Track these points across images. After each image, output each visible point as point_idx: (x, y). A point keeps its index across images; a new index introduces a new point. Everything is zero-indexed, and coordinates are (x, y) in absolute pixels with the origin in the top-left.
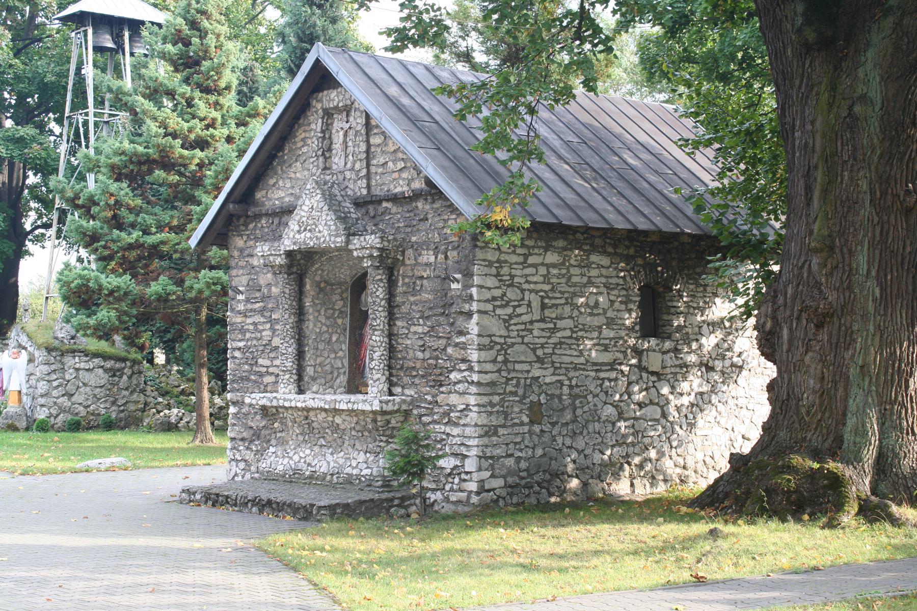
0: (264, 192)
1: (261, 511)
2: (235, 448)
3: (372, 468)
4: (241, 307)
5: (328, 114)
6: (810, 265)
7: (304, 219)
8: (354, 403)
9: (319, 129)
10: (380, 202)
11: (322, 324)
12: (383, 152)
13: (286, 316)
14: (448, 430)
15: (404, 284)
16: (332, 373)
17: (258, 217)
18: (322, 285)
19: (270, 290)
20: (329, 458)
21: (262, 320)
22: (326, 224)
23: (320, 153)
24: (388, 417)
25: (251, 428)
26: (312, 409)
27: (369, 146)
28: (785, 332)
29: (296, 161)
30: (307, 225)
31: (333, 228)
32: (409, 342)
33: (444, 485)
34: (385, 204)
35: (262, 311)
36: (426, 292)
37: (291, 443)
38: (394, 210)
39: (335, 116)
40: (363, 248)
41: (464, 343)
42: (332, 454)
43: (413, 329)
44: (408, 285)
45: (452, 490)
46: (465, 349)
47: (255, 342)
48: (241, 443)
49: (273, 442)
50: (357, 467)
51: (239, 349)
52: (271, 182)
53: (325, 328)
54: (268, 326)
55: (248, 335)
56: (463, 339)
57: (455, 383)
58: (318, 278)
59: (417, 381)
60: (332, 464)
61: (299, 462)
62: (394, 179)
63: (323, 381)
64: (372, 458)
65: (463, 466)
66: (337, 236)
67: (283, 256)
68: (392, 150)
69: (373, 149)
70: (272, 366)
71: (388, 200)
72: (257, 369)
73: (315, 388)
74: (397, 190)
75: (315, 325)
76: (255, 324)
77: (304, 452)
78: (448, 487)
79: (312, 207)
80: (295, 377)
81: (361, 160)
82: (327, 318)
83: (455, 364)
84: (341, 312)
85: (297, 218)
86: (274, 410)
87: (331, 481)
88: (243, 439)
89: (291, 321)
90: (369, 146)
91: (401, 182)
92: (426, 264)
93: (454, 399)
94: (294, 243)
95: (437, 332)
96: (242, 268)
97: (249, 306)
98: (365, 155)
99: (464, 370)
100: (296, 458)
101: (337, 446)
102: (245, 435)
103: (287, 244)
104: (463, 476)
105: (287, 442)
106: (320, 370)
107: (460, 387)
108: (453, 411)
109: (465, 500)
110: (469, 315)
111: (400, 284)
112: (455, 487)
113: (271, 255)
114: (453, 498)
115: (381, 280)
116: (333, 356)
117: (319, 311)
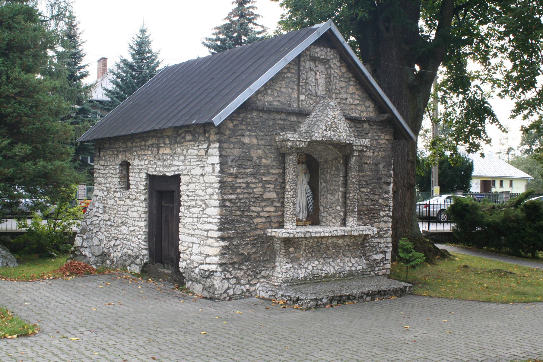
1: (373, 299)
2: (225, 270)
3: (362, 265)
7: (330, 123)
8: (363, 231)
14: (378, 240)
19: (260, 161)
20: (333, 264)
21: (254, 180)
25: (243, 254)
26: (324, 237)
35: (254, 175)
37: (301, 259)
40: (361, 146)
41: (388, 197)
42: (333, 261)
43: (362, 190)
45: (380, 270)
46: (388, 200)
47: (247, 196)
50: (353, 266)
54: (260, 185)
55: (239, 191)
56: (387, 196)
59: (363, 217)
60: (336, 268)
61: (313, 269)
64: (359, 260)
66: (351, 137)
68: (351, 92)
70: (263, 211)
72: (249, 214)
74: (353, 115)
77: (314, 263)
78: (377, 269)
79: (335, 118)
87: (340, 277)
88: (233, 264)
91: (357, 111)
92: (368, 157)
94: (323, 137)
95: (375, 192)
97: (243, 171)
100: (310, 268)
101: (334, 256)
105: (299, 259)
107: (385, 219)
108: (381, 231)
112: (381, 268)
114: (380, 274)
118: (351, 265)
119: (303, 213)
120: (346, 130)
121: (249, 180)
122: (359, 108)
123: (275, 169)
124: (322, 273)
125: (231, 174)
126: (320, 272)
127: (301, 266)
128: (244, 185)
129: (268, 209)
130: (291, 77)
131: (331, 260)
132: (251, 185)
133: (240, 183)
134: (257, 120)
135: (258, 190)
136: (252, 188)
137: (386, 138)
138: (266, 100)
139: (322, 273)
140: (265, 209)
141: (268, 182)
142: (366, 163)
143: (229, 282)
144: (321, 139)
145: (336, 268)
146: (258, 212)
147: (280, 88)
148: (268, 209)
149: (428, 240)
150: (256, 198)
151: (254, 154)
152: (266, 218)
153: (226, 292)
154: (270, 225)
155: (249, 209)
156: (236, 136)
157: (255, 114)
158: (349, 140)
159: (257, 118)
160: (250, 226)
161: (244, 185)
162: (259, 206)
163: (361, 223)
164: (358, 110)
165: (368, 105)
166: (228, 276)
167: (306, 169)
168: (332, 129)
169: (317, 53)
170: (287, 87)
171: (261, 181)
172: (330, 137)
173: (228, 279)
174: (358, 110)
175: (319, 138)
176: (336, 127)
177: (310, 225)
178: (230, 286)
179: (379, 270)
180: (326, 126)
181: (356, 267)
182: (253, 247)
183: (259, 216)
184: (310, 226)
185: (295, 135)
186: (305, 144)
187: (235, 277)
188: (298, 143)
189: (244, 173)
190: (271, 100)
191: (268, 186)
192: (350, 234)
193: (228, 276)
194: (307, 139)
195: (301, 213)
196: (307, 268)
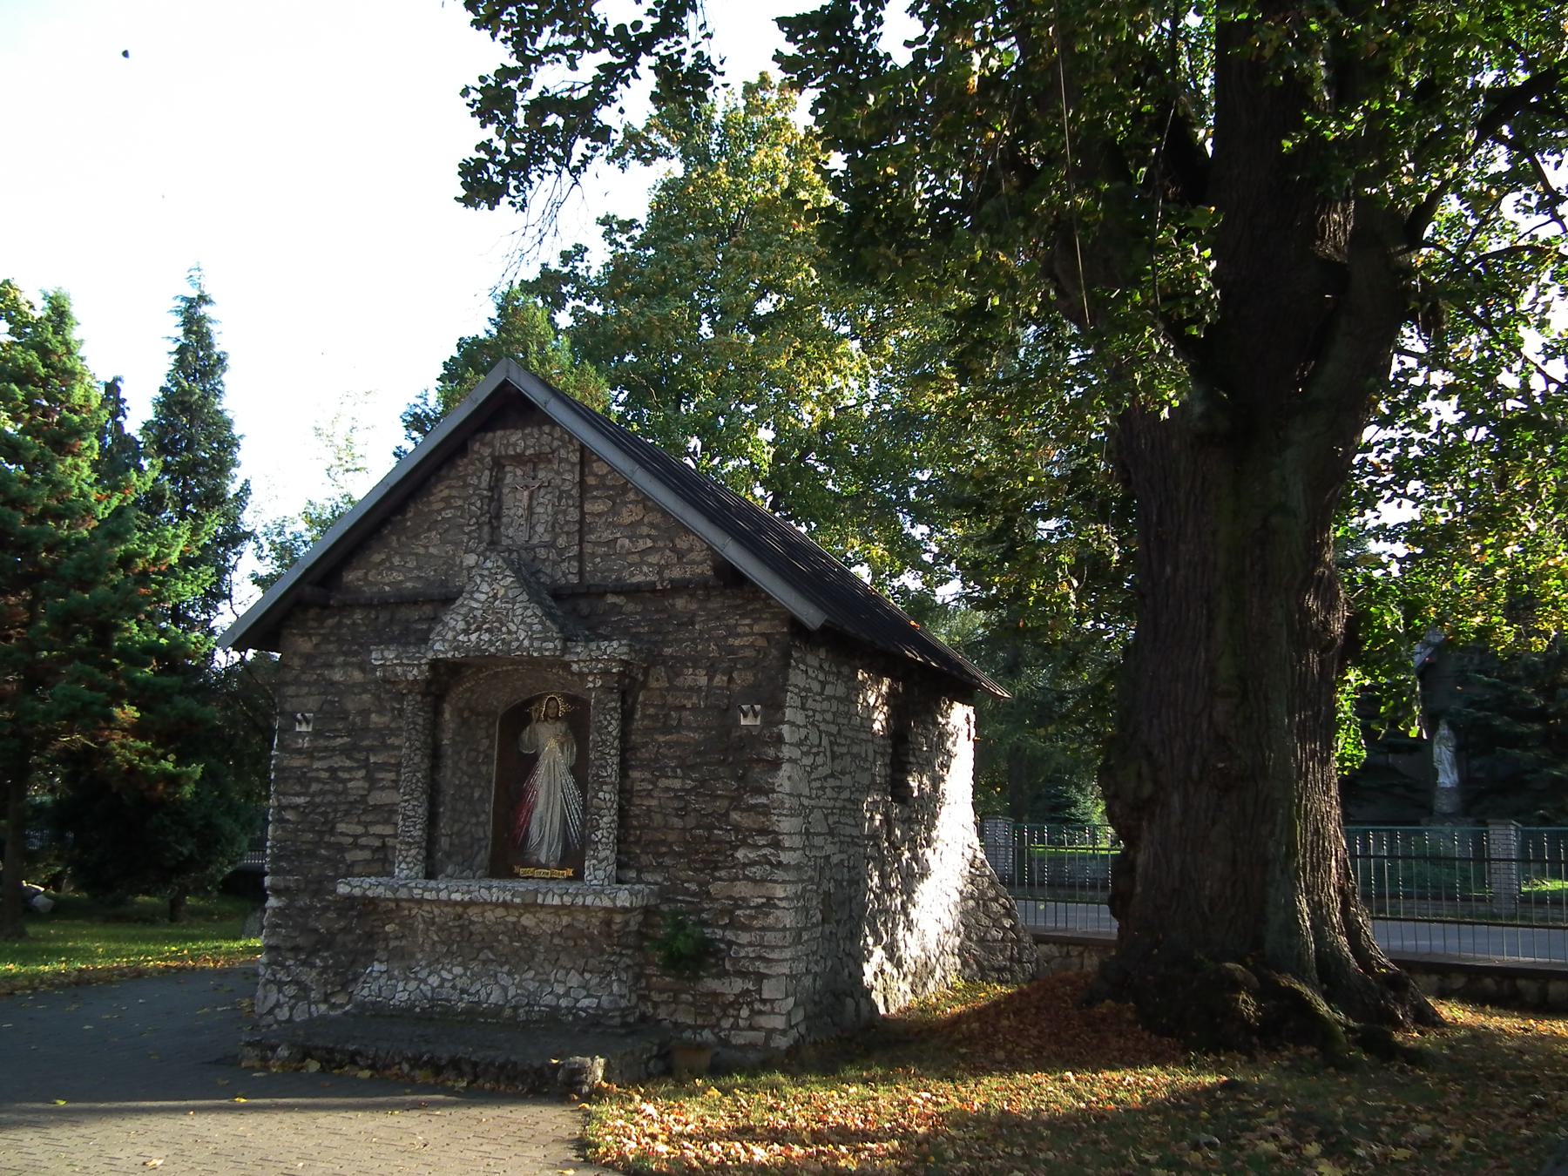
0: (360, 573)
2: (276, 963)
4: (305, 743)
5: (498, 464)
6: (1210, 716)
9: (484, 485)
10: (602, 594)
11: (464, 773)
12: (609, 525)
13: (417, 759)
14: (729, 935)
15: (644, 716)
16: (471, 846)
17: (347, 607)
18: (466, 715)
20: (504, 980)
21: (348, 763)
22: (522, 622)
23: (485, 519)
24: (628, 916)
27: (583, 514)
28: (1176, 800)
29: (429, 530)
31: (537, 627)
32: (654, 803)
33: (719, 1020)
34: (611, 599)
35: (346, 751)
36: (690, 728)
37: (419, 956)
38: (630, 607)
39: (508, 468)
41: (765, 805)
42: (509, 973)
43: (663, 783)
44: (654, 717)
45: (735, 1026)
47: (330, 797)
48: (289, 955)
49: (381, 954)
50: (567, 994)
51: (296, 807)
52: (377, 558)
53: (466, 779)
54: (361, 773)
55: (314, 787)
57: (745, 866)
58: (461, 704)
59: (668, 861)
61: (441, 986)
62: (630, 565)
63: (460, 858)
64: (596, 980)
65: (759, 991)
67: (425, 668)
69: (588, 519)
70: (366, 834)
71: (616, 593)
73: (449, 870)
74: (635, 580)
75: (454, 774)
76: (332, 771)
77: (450, 971)
78: (726, 1023)
79: (495, 597)
80: (423, 852)
81: (568, 533)
82: (470, 764)
83: (745, 838)
84: (487, 756)
85: (463, 610)
86: (393, 905)
89: (423, 766)
90: (583, 514)
92: (691, 689)
93: (742, 889)
94: (456, 649)
96: (307, 684)
97: (322, 743)
98: (577, 527)
99: (764, 846)
102: (300, 941)
103: (440, 648)
104: (757, 1006)
105: (412, 956)
106: (456, 841)
108: (740, 908)
109: (761, 1042)
110: (776, 764)
111: (637, 716)
113: (401, 664)
115: (614, 709)
116: (474, 820)
117: (459, 753)
118: (560, 990)
119: (550, 846)
121: (338, 761)
122: (653, 559)
124: (461, 1000)
125: (300, 751)
127: (408, 973)
128: (324, 775)
129: (378, 829)
130: (454, 517)
131: (506, 968)
132: (340, 774)
133: (317, 770)
135: (357, 784)
136: (344, 781)
137: (756, 628)
139: (461, 1000)
140: (372, 830)
143: (280, 991)
146: (356, 837)
147: (426, 547)
148: (378, 829)
151: (351, 705)
152: (376, 850)
153: (271, 1012)
155: (333, 828)
156: (314, 668)
157: (358, 616)
158: (539, 649)
160: (336, 869)
161: (324, 775)
162: (359, 823)
164: (650, 565)
166: (282, 976)
167: (565, 734)
169: (515, 445)
170: (444, 542)
171: (365, 764)
172: (477, 647)
173: (280, 985)
174: (650, 565)
175: (445, 652)
178: (282, 1000)
179: (732, 1028)
180: (467, 623)
181: (577, 1001)
182: (340, 916)
183: (355, 845)
185: (386, 653)
186: (421, 672)
187: (297, 983)
188: (399, 670)
189: (326, 749)
191: (380, 776)
192: (529, 900)
193: (282, 976)
195: (545, 847)
196: (424, 981)
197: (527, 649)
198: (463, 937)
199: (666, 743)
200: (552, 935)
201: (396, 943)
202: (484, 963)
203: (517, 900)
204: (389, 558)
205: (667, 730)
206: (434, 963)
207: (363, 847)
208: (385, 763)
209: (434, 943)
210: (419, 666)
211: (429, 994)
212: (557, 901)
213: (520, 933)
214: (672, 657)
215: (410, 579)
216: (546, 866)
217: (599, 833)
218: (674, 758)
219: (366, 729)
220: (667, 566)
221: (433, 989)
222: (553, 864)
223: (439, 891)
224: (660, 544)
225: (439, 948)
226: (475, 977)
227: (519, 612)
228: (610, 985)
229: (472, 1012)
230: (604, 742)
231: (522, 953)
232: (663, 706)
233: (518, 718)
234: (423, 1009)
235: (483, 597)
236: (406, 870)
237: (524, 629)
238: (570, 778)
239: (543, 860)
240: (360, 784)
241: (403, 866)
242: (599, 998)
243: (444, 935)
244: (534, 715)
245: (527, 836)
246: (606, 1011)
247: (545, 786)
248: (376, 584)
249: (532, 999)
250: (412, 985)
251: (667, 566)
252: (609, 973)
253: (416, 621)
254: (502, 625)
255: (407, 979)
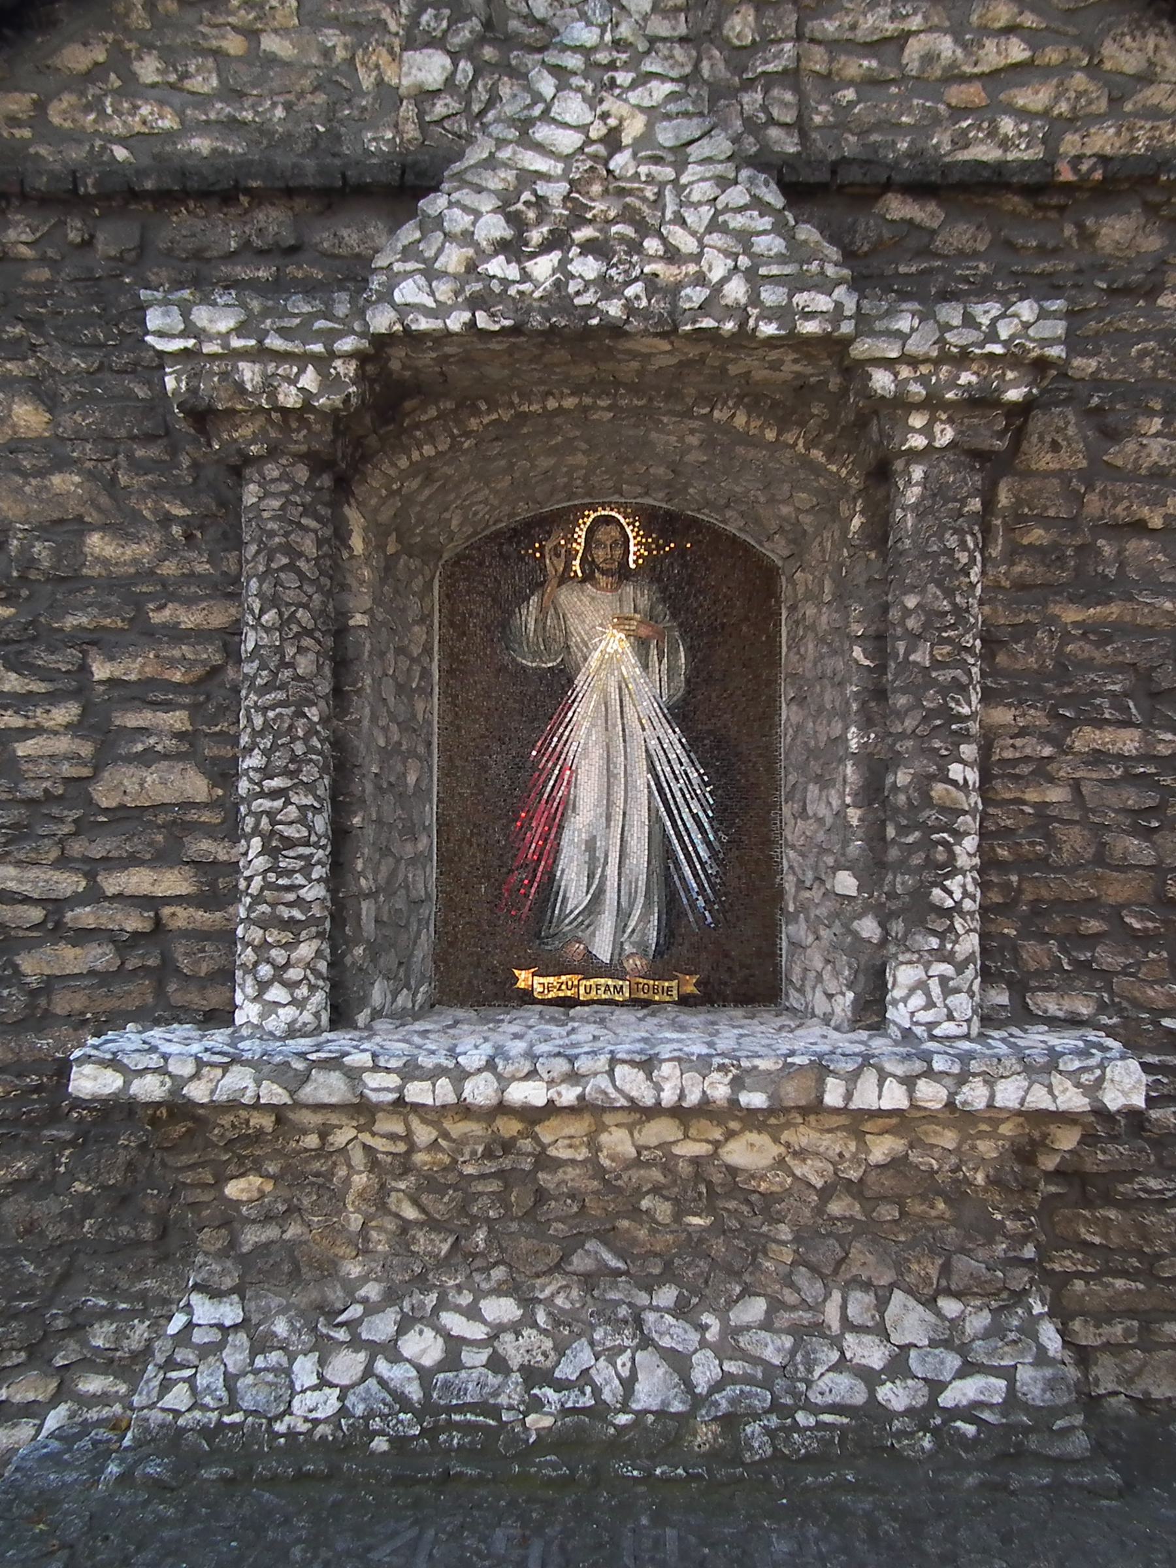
13: (305, 665)
20: (674, 1333)
22: (714, 226)
30: (578, 218)
32: (1056, 795)
34: (898, 208)
42: (681, 1310)
43: (1086, 738)
50: (898, 1367)
52: (79, 57)
54: (64, 714)
59: (1107, 958)
60: (705, 1370)
62: (958, 112)
64: (979, 1321)
67: (345, 369)
70: (93, 895)
71: (919, 189)
77: (473, 1313)
79: (612, 141)
85: (496, 181)
86: (267, 1122)
91: (1007, 125)
94: (474, 303)
105: (328, 1269)
113: (261, 354)
118: (875, 1356)
119: (622, 915)
120: (745, 238)
122: (1033, 97)
123: (189, 602)
124: (536, 1405)
126: (512, 1393)
127: (322, 1327)
129: (138, 881)
131: (667, 1296)
134: (45, 274)
138: (116, 126)
139: (536, 1405)
140: (112, 883)
141: (142, 693)
142: (1139, 527)
144: (456, 322)
145: (705, 1370)
146: (56, 905)
147: (251, 34)
148: (138, 881)
149: (1119, 1329)
150: (31, 802)
152: (126, 944)
154: (160, 991)
158: (782, 314)
159: (43, 260)
162: (63, 862)
163: (1085, 1009)
164: (1023, 114)
165: (1131, 63)
167: (651, 617)
168: (583, 234)
171: (78, 685)
174: (1023, 114)
175: (440, 311)
176: (629, 215)
177: (685, 1001)
180: (515, 220)
181: (936, 1387)
183: (55, 928)
184: (695, 1019)
185: (202, 316)
186: (329, 382)
188: (249, 373)
190: (168, 122)
191: (132, 720)
192: (793, 1094)
194: (330, 336)
195: (607, 923)
197: (739, 312)
198: (507, 1202)
199: (1087, 630)
200: (826, 1194)
201: (271, 1233)
202: (588, 1281)
203: (755, 1099)
204: (120, 61)
205: (1092, 590)
206: (411, 1287)
207: (82, 936)
208: (148, 683)
209: (405, 1226)
210: (322, 362)
211: (414, 1392)
212: (894, 1097)
213: (711, 1185)
214: (1096, 382)
215: (206, 127)
216: (613, 970)
217: (954, 884)
218: (1121, 668)
219: (69, 581)
220: (1071, 122)
221: (425, 1375)
222: (635, 963)
223: (460, 1076)
224: (1053, 55)
225: (422, 1242)
226: (566, 1329)
227: (701, 191)
228: (1029, 1329)
229: (580, 1436)
230: (957, 611)
231: (718, 1247)
232: (1073, 524)
233: (505, 564)
234: (399, 1443)
235: (568, 141)
236: (272, 1010)
237: (723, 251)
238: (672, 738)
239: (603, 951)
240: (63, 744)
241: (276, 993)
242: (1008, 1373)
243: (440, 1207)
244: (552, 566)
245: (549, 887)
246: (1044, 1417)
247: (596, 754)
248: (76, 137)
249: (785, 1385)
250: (347, 1366)
251: (1071, 122)
252: (1019, 1297)
253: (230, 257)
254: (644, 229)
255: (324, 1349)
